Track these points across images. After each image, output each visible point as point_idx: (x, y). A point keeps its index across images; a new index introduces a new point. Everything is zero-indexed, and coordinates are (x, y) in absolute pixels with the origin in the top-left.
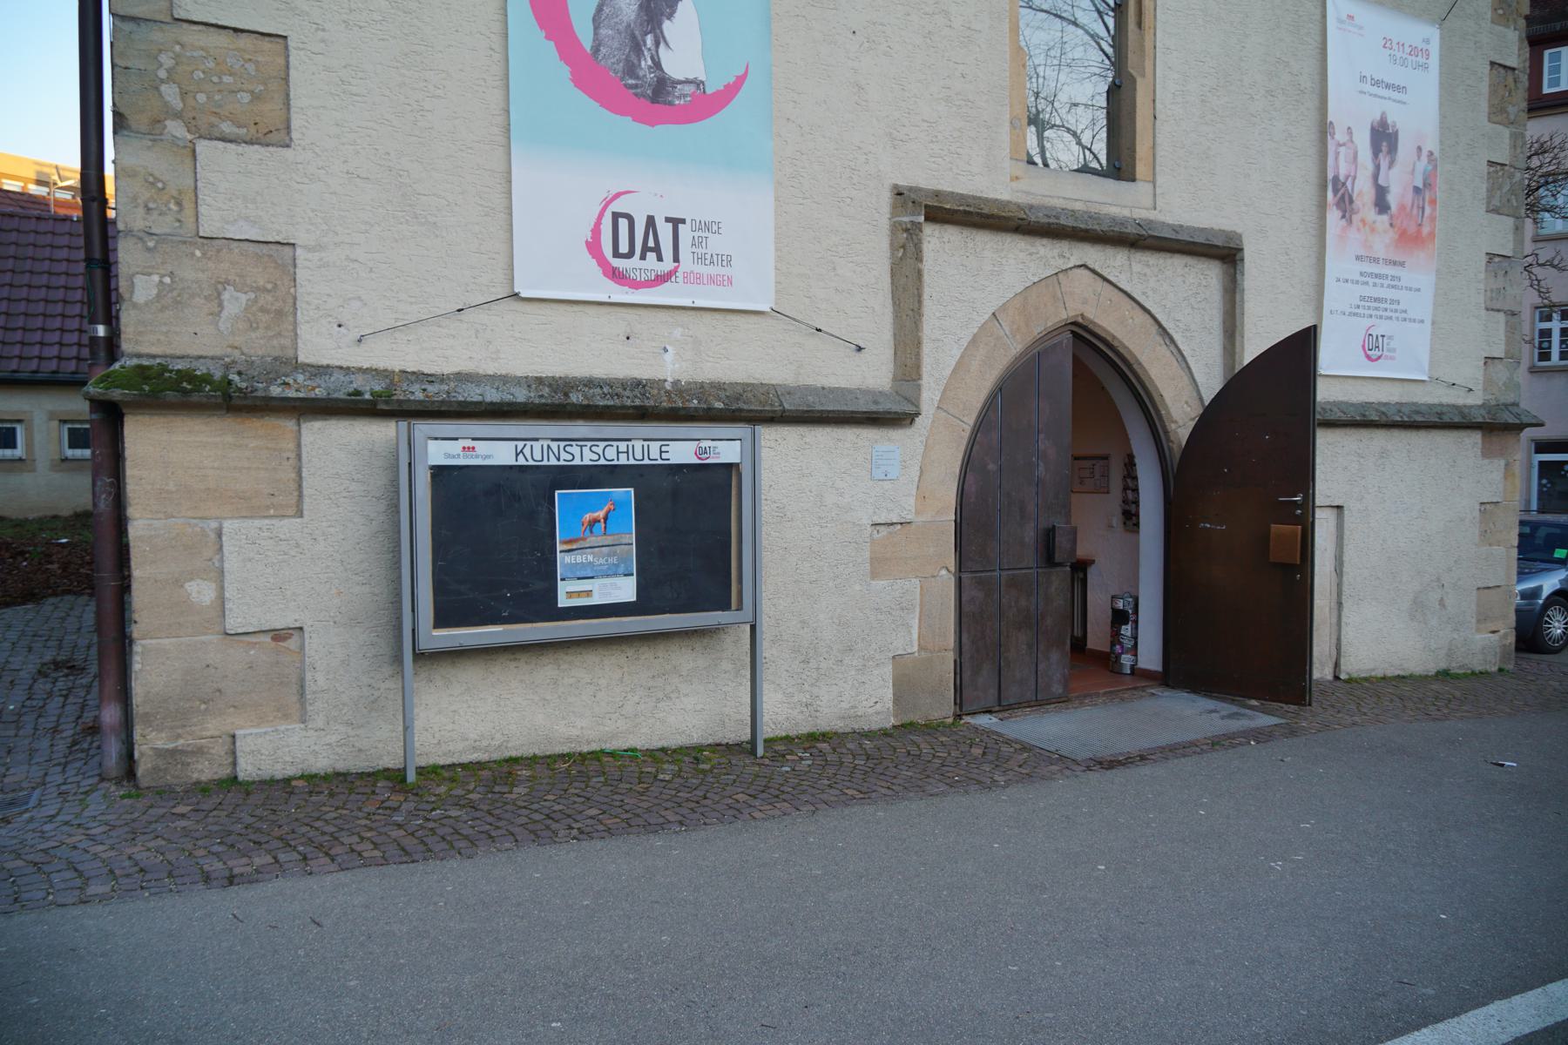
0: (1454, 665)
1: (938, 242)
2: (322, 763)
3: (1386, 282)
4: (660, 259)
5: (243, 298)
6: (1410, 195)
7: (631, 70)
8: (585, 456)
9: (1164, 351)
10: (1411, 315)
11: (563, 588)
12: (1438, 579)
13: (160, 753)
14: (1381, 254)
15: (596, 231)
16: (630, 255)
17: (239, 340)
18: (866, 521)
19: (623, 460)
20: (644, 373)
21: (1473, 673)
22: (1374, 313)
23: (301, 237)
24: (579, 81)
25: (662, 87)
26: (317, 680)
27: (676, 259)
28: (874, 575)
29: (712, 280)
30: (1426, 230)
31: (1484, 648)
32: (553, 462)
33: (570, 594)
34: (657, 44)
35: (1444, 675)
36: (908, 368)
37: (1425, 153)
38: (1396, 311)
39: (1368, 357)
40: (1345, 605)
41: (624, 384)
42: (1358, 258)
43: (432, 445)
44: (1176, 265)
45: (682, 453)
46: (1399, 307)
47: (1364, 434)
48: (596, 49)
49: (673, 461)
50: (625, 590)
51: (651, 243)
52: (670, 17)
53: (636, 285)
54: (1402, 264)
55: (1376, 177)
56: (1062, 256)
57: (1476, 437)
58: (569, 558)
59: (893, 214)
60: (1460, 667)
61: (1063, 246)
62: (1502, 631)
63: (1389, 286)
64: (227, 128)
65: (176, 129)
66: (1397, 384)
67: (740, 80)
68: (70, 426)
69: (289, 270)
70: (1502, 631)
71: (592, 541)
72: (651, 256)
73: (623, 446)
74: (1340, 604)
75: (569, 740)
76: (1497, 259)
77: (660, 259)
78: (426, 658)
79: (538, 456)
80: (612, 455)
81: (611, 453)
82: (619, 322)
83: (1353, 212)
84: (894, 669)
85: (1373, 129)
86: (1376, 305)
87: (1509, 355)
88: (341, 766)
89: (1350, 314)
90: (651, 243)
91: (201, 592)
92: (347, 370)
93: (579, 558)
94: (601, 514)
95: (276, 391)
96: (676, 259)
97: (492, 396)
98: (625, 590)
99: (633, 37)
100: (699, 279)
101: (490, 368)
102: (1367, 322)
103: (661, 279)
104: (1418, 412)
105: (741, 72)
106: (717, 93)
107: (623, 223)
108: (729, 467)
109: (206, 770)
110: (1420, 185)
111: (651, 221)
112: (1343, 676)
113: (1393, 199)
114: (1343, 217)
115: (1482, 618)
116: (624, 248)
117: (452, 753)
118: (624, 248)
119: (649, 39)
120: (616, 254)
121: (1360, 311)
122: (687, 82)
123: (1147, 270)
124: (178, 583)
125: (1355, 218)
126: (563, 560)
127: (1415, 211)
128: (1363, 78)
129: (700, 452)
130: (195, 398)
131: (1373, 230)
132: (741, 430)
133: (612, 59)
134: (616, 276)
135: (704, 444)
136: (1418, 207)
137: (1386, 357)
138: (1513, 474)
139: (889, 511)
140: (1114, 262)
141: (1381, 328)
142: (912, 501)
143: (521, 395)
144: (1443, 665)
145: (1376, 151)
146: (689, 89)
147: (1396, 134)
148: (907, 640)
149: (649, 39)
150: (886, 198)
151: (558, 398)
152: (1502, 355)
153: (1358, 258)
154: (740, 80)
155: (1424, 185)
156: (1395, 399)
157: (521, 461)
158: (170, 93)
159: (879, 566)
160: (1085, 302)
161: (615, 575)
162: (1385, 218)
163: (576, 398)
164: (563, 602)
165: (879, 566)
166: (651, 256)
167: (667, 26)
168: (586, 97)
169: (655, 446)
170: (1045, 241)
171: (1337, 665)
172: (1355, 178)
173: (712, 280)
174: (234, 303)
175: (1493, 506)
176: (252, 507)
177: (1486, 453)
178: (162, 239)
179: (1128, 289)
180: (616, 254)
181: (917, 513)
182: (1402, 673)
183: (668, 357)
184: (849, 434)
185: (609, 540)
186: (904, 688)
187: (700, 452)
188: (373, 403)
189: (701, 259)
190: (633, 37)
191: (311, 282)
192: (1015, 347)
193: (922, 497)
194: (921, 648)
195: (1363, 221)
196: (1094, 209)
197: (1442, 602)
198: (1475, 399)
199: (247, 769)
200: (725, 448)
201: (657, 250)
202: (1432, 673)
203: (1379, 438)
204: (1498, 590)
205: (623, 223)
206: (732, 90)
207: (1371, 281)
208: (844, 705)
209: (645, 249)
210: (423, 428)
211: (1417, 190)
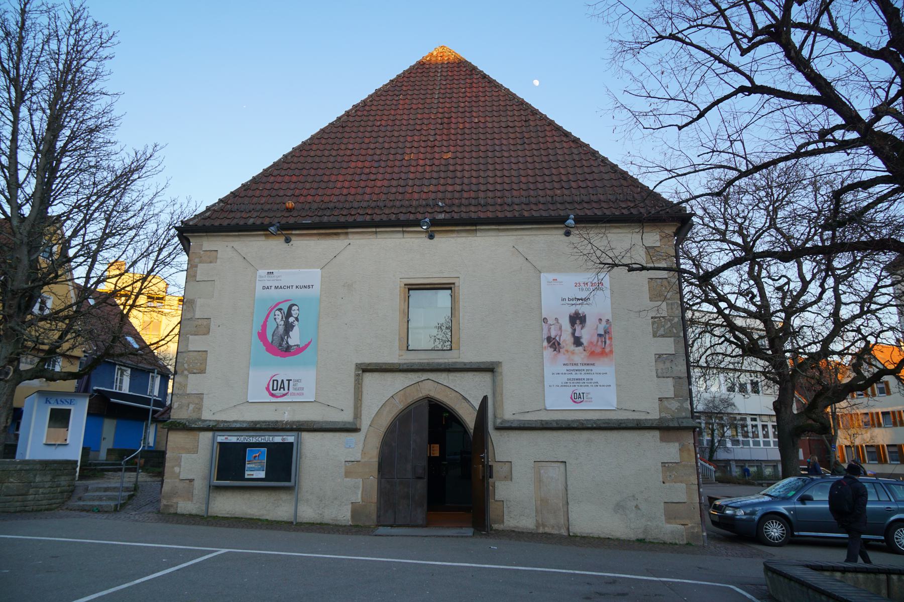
0: (649, 537)
1: (368, 378)
2: (194, 512)
3: (583, 372)
4: (284, 390)
5: (193, 406)
6: (595, 338)
7: (280, 345)
8: (253, 440)
9: (465, 404)
10: (600, 384)
11: (247, 473)
13: (164, 505)
14: (579, 362)
15: (268, 385)
16: (277, 390)
17: (191, 415)
18: (343, 461)
19: (263, 441)
20: (279, 419)
21: (665, 543)
22: (572, 384)
23: (205, 392)
24: (268, 350)
25: (289, 347)
26: (196, 492)
27: (288, 390)
28: (346, 476)
29: (298, 394)
30: (607, 350)
32: (246, 441)
33: (248, 475)
34: (288, 338)
36: (357, 414)
38: (591, 383)
40: (570, 503)
41: (272, 422)
42: (564, 365)
43: (218, 437)
44: (469, 376)
45: (278, 439)
46: (593, 381)
48: (272, 342)
49: (276, 441)
50: (262, 475)
51: (282, 386)
52: (291, 331)
53: (277, 397)
54: (593, 364)
55: (573, 334)
56: (419, 377)
57: (657, 434)
58: (249, 466)
59: (355, 371)
60: (654, 539)
61: (419, 374)
63: (585, 373)
64: (195, 371)
65: (186, 372)
67: (309, 343)
68: (221, 439)
69: (202, 399)
70: (690, 525)
71: (255, 461)
72: (282, 390)
73: (263, 437)
74: (568, 503)
75: (250, 514)
76: (665, 356)
77: (284, 390)
78: (218, 488)
80: (260, 440)
81: (260, 439)
82: (273, 407)
83: (560, 348)
84: (352, 508)
85: (570, 316)
86: (578, 381)
88: (198, 513)
89: (562, 386)
90: (282, 386)
91: (177, 469)
92: (210, 421)
93: (251, 466)
94: (257, 455)
95: (193, 426)
96: (288, 390)
97: (238, 425)
98: (262, 475)
99: (282, 337)
100: (294, 394)
101: (241, 419)
102: (574, 388)
103: (284, 395)
105: (309, 340)
106: (303, 347)
107: (275, 382)
108: (292, 443)
109: (172, 511)
110: (602, 333)
111: (283, 381)
112: (571, 534)
113: (584, 340)
114: (555, 350)
116: (275, 388)
117: (222, 514)
118: (275, 388)
119: (286, 337)
120: (273, 390)
121: (568, 384)
122: (295, 345)
123: (456, 378)
124: (173, 467)
126: (247, 466)
127: (600, 343)
128: (563, 300)
129: (283, 439)
130: (178, 427)
132: (295, 433)
133: (276, 344)
134: (272, 395)
135: (284, 437)
136: (602, 341)
137: (586, 401)
139: (351, 457)
140: (442, 378)
141: (580, 390)
142: (360, 455)
143: (245, 425)
144: (641, 536)
146: (295, 347)
147: (585, 316)
148: (358, 498)
149: (286, 337)
150: (353, 367)
151: (254, 426)
152: (673, 396)
154: (309, 343)
155: (605, 332)
157: (238, 441)
158: (186, 365)
159: (348, 474)
160: (430, 390)
161: (260, 470)
162: (580, 348)
163: (258, 426)
164: (246, 477)
165: (348, 474)
166: (282, 390)
167: (291, 333)
169: (271, 438)
170: (412, 373)
171: (568, 529)
172: (561, 336)
173: (298, 394)
174: (191, 407)
176: (189, 451)
177: (662, 440)
178: (180, 395)
179: (447, 385)
180: (273, 390)
181: (362, 458)
182: (610, 537)
183: (286, 414)
184: (337, 434)
185: (259, 461)
186: (355, 513)
187: (283, 439)
188: (212, 428)
189: (295, 389)
190: (282, 337)
191: (206, 403)
192: (401, 407)
193: (364, 453)
194: (362, 502)
196: (431, 361)
197: (637, 507)
199: (179, 511)
200: (290, 439)
201: (284, 388)
203: (586, 435)
205: (275, 382)
206: (307, 346)
208: (333, 516)
209: (281, 388)
210: (217, 433)
211: (600, 335)
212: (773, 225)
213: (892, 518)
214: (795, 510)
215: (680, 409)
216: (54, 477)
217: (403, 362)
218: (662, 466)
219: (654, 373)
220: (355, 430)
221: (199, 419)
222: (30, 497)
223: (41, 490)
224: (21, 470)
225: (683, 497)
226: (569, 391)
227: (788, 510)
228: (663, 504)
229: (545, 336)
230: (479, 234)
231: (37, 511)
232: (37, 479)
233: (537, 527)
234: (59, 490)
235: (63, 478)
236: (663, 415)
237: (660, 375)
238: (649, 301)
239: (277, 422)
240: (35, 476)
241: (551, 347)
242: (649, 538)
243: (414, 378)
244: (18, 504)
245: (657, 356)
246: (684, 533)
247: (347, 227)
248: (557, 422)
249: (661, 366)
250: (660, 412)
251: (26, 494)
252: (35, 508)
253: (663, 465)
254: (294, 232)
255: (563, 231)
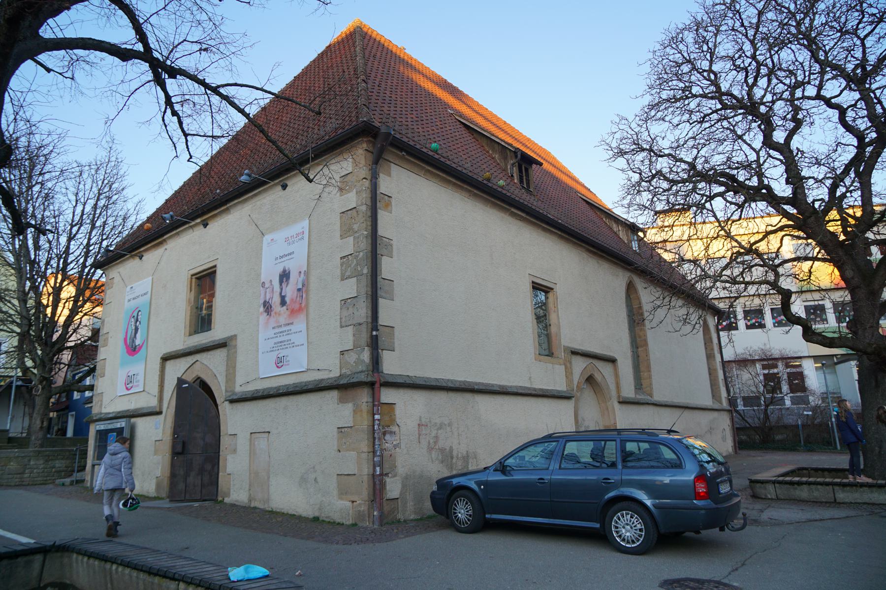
0: (323, 515)
3: (285, 334)
10: (297, 343)
12: (314, 468)
21: (334, 522)
31: (341, 509)
35: (316, 519)
37: (303, 273)
39: (278, 367)
42: (273, 328)
47: (278, 400)
54: (292, 324)
57: (335, 394)
60: (327, 517)
62: (358, 502)
66: (294, 375)
70: (358, 502)
76: (349, 301)
79: (817, 249)
87: (355, 346)
102: (277, 352)
104: (296, 387)
110: (301, 287)
113: (287, 299)
115: (156, 452)
125: (273, 313)
127: (298, 299)
131: (279, 315)
138: (361, 411)
144: (317, 514)
145: (281, 282)
152: (352, 348)
153: (273, 328)
156: (291, 382)
168: (306, 63)
175: (349, 429)
186: (158, 486)
195: (276, 313)
197: (315, 479)
198: (335, 373)
202: (311, 517)
203: (302, 399)
204: (354, 477)
207: (278, 335)
211: (299, 290)
212: (863, 41)
213: (612, 494)
214: (486, 483)
215: (359, 361)
216: (47, 461)
217: (186, 347)
218: (339, 432)
219: (338, 324)
220: (159, 413)
221: (101, 413)
222: (26, 476)
223: (35, 471)
224: (18, 457)
225: (351, 468)
226: (274, 356)
227: (479, 483)
228: (336, 476)
229: (262, 301)
230: (232, 211)
231: (32, 485)
232: (32, 463)
233: (250, 501)
234: (54, 470)
235: (57, 461)
236: (344, 371)
237: (343, 324)
238: (339, 241)
239: (128, 410)
240: (29, 461)
241: (265, 311)
242: (323, 517)
243: (190, 360)
244: (17, 480)
245: (343, 302)
246: (351, 512)
247: (162, 235)
248: (278, 388)
249: (345, 313)
250: (341, 369)
251: (23, 473)
252: (31, 483)
253: (340, 430)
254: (142, 249)
255: (280, 188)
